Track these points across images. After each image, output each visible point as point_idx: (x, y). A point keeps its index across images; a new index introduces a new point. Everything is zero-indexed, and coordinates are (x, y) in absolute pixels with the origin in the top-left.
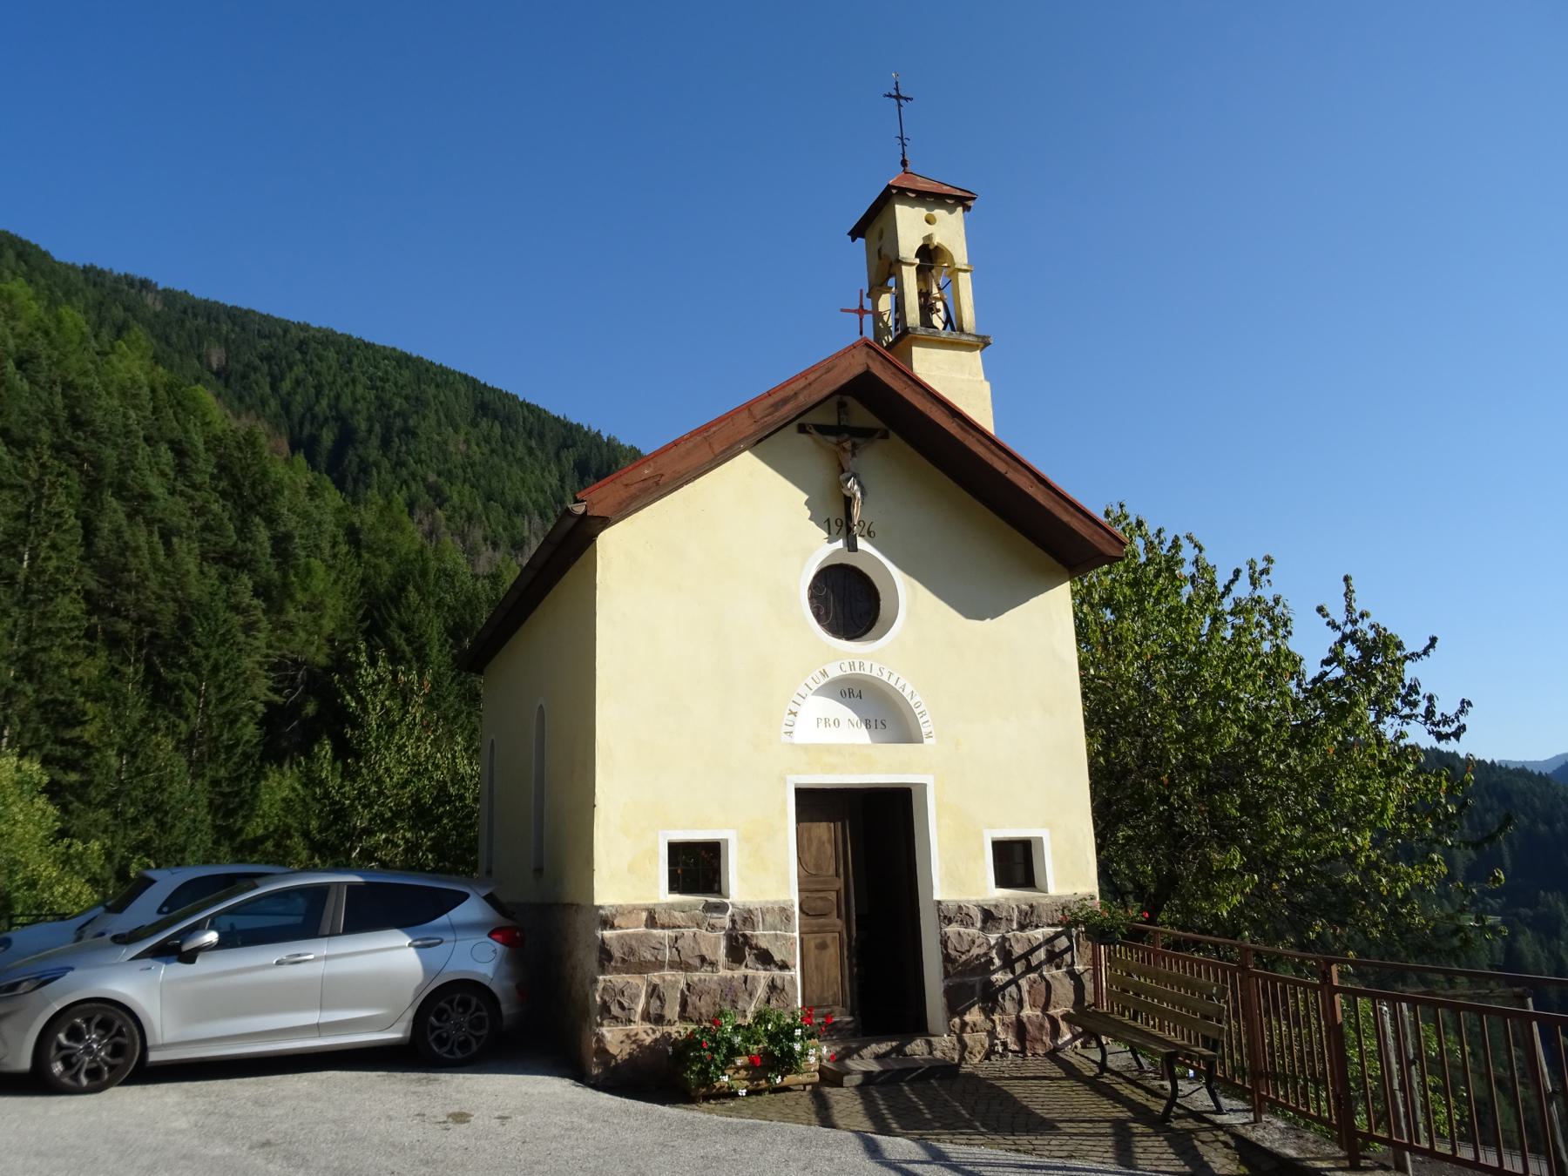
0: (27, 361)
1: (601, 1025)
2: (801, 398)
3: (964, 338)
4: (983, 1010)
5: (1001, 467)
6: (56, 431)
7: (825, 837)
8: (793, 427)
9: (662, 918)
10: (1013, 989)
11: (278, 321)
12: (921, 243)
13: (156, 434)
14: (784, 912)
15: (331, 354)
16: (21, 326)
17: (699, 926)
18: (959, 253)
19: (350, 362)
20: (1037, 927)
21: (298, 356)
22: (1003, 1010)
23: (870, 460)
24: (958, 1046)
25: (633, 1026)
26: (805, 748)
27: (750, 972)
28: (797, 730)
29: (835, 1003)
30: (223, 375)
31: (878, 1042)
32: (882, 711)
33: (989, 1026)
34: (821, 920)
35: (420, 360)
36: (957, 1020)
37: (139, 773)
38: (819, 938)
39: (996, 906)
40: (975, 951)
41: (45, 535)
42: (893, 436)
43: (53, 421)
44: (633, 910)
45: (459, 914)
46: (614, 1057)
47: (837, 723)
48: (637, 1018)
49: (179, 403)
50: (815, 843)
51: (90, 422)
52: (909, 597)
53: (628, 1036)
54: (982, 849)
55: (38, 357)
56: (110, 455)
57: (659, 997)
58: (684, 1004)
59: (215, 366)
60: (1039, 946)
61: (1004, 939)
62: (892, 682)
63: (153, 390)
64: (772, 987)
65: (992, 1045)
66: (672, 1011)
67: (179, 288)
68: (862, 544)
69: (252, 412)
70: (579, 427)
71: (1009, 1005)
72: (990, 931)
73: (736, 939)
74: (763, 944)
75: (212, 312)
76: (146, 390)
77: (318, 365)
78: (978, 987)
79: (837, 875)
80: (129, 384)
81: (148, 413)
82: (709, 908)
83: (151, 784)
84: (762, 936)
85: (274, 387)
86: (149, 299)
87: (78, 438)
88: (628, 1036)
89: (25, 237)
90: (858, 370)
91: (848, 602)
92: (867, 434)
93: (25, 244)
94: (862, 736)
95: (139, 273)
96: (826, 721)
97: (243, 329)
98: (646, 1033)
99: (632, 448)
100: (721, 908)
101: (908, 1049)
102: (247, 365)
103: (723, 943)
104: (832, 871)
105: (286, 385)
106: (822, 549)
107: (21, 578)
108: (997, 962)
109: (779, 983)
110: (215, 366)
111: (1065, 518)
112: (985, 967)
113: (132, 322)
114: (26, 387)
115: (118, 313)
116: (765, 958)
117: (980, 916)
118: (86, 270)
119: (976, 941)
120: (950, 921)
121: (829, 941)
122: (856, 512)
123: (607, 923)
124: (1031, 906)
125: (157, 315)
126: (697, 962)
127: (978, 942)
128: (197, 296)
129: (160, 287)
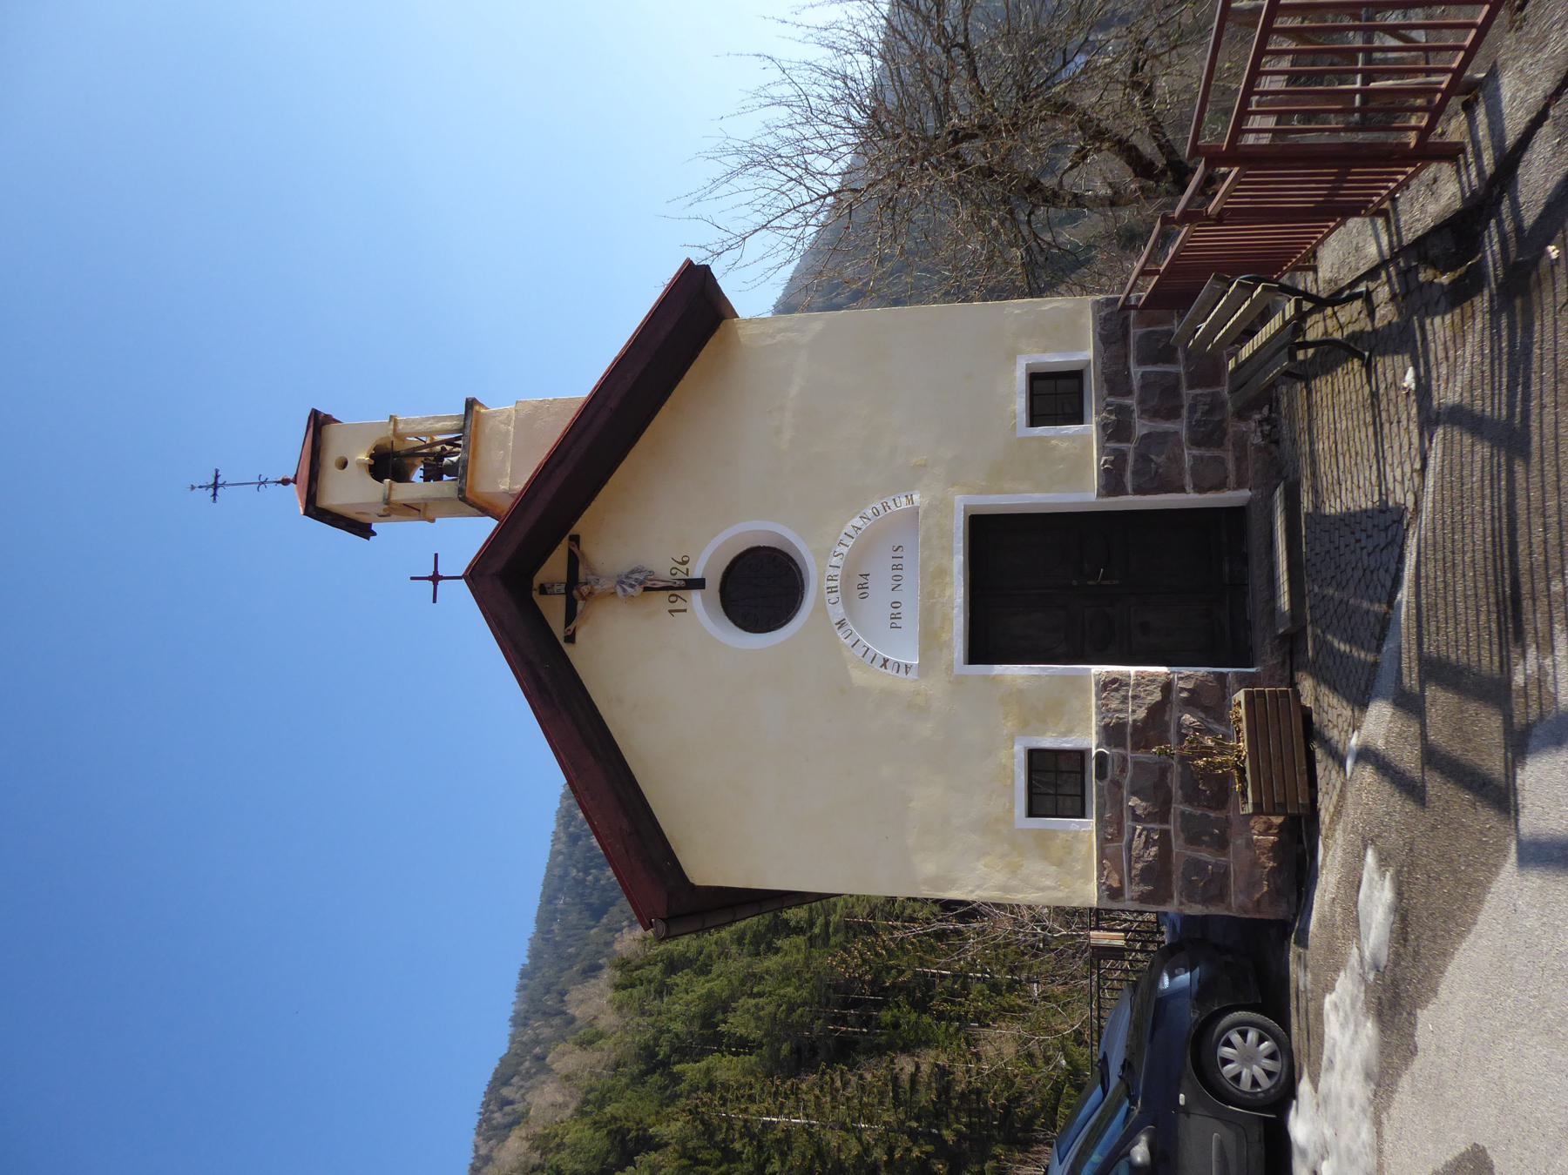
42: (577, 528)
47: (896, 604)
54: (1040, 439)
82: (1101, 775)
84: (1135, 714)
89: (489, 1077)
91: (762, 588)
92: (574, 561)
93: (495, 1079)
96: (894, 617)
113: (560, 987)
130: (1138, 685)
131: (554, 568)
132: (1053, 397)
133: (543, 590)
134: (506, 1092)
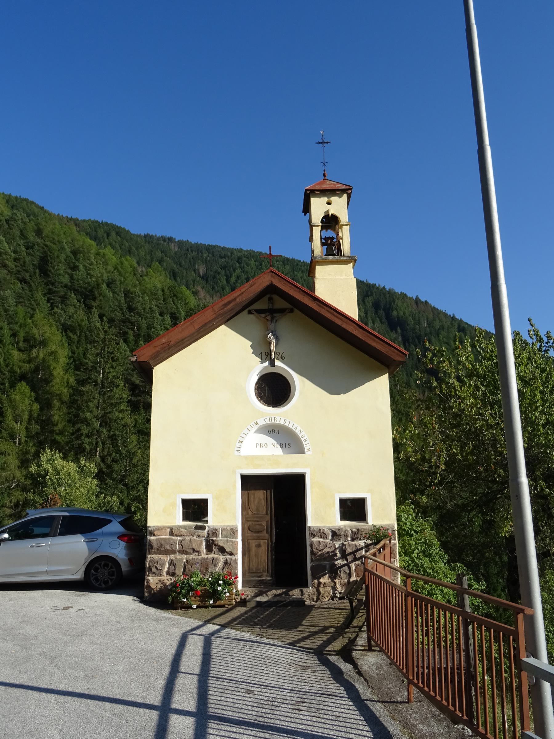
0: (111, 283)
1: (148, 576)
2: (238, 300)
3: (342, 258)
4: (330, 577)
5: (339, 322)
6: (123, 313)
7: (262, 497)
8: (246, 311)
9: (175, 532)
10: (346, 568)
11: (228, 249)
12: (323, 215)
13: (165, 311)
14: (233, 532)
15: (252, 262)
16: (110, 268)
17: (192, 535)
18: (344, 218)
19: (261, 265)
20: (360, 539)
21: (237, 265)
22: (341, 578)
23: (284, 325)
24: (316, 593)
25: (162, 577)
26: (246, 457)
27: (216, 556)
28: (242, 449)
29: (264, 571)
30: (205, 278)
31: (276, 589)
32: (289, 440)
33: (332, 584)
34: (259, 534)
35: (293, 260)
36: (316, 581)
37: (135, 466)
38: (257, 542)
39: (339, 529)
40: (327, 550)
41: (107, 362)
42: (295, 310)
43: (121, 309)
44: (163, 528)
45: (107, 529)
46: (153, 589)
47: (266, 445)
48: (165, 573)
49: (175, 295)
50: (256, 501)
51: (136, 308)
52: (301, 385)
53: (160, 581)
55: (115, 281)
56: (144, 323)
57: (174, 565)
58: (185, 569)
59: (201, 274)
60: (362, 549)
61: (343, 545)
62: (290, 426)
63: (163, 291)
64: (226, 563)
65: (334, 594)
66: (180, 571)
67: (185, 239)
68: (277, 363)
69: (218, 294)
70: (374, 285)
71: (343, 575)
72: (336, 541)
73: (209, 542)
74: (221, 544)
75: (199, 249)
76: (160, 291)
77: (247, 268)
78: (328, 567)
79: (267, 514)
80: (153, 289)
81: (162, 302)
82: (197, 528)
83: (140, 471)
84: (220, 540)
85: (228, 281)
86: (172, 246)
87: (131, 316)
88: (160, 581)
90: (268, 283)
91: (274, 390)
92: (282, 311)
94: (278, 451)
95: (167, 235)
97: (213, 255)
98: (167, 580)
99: (402, 293)
100: (203, 528)
101: (291, 593)
102: (215, 272)
103: (204, 543)
104: (265, 512)
105: (233, 280)
106: (257, 368)
107: (99, 381)
108: (339, 555)
109: (229, 561)
110: (201, 274)
111: (374, 344)
112: (332, 557)
113: (165, 258)
114: (111, 295)
115: (159, 254)
116: (222, 550)
117: (330, 534)
118: (146, 236)
119: (326, 544)
120: (314, 536)
121: (262, 544)
122: (273, 348)
123: (152, 534)
124: (358, 530)
125: (175, 253)
126: (191, 551)
127: (328, 546)
128: (193, 242)
129: (176, 240)
130: (233, 542)
131: (280, 303)
132: (354, 509)
133: (270, 299)
134: (113, 234)
